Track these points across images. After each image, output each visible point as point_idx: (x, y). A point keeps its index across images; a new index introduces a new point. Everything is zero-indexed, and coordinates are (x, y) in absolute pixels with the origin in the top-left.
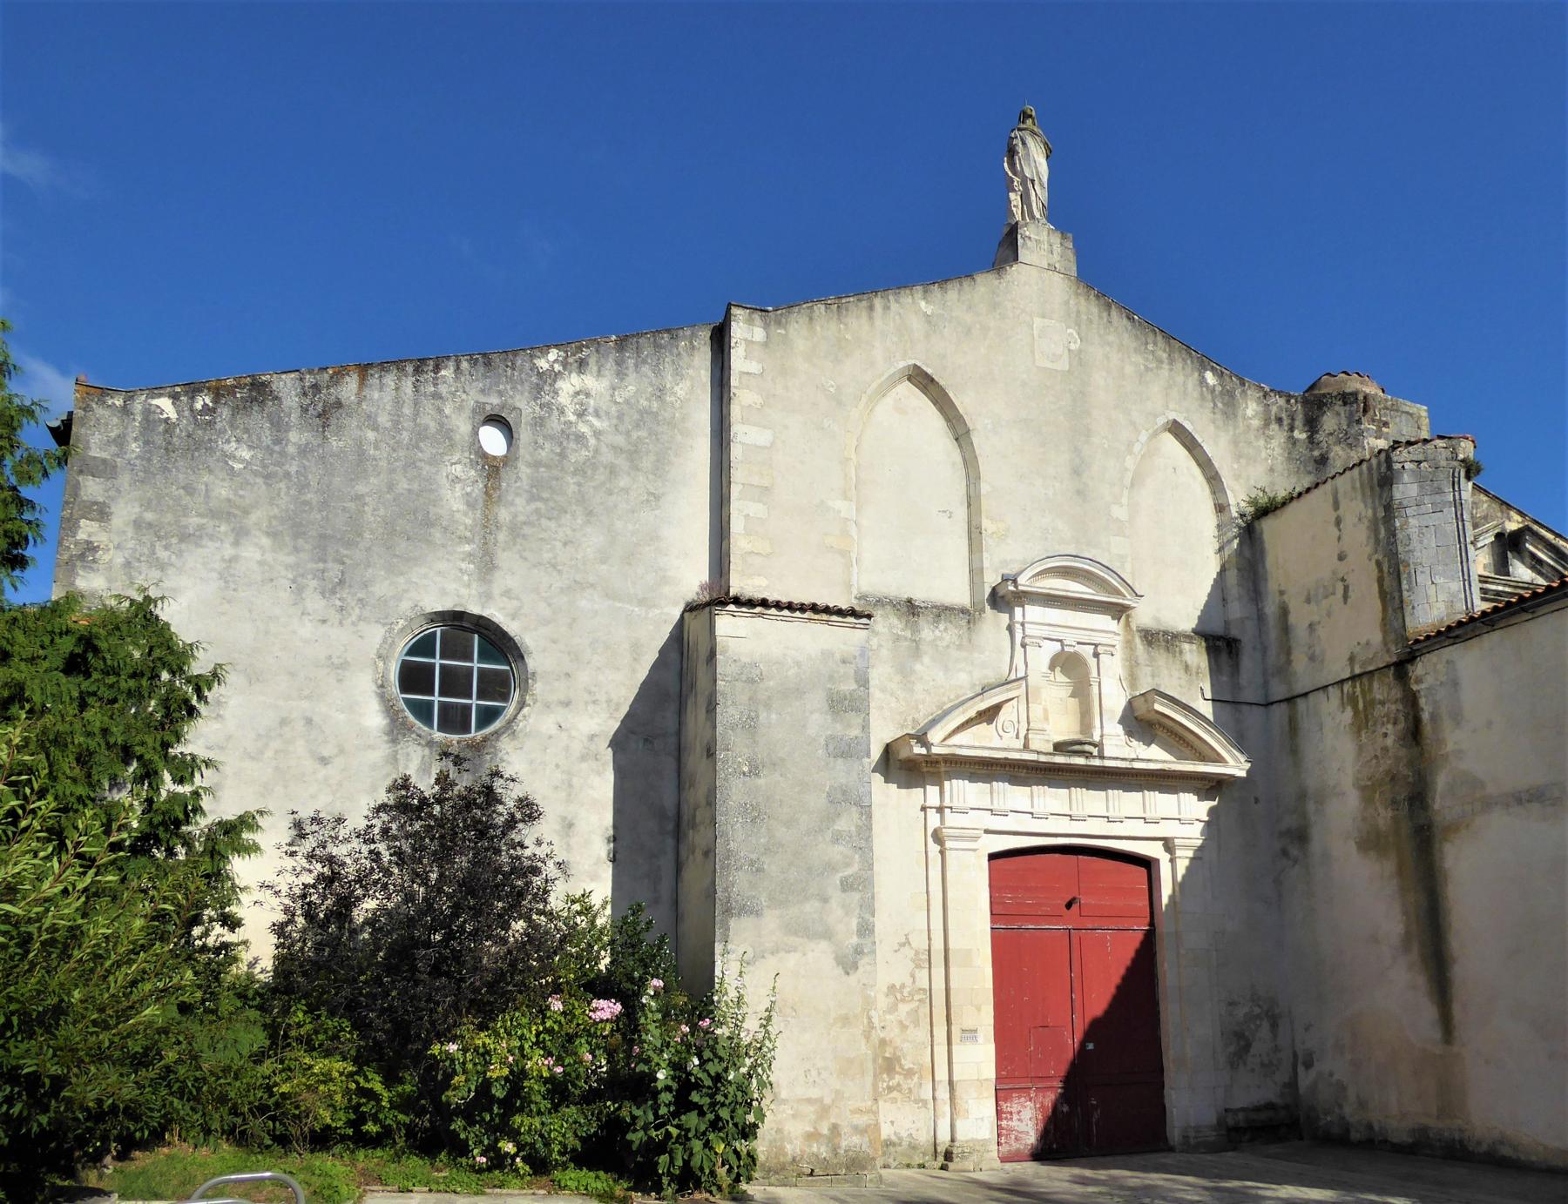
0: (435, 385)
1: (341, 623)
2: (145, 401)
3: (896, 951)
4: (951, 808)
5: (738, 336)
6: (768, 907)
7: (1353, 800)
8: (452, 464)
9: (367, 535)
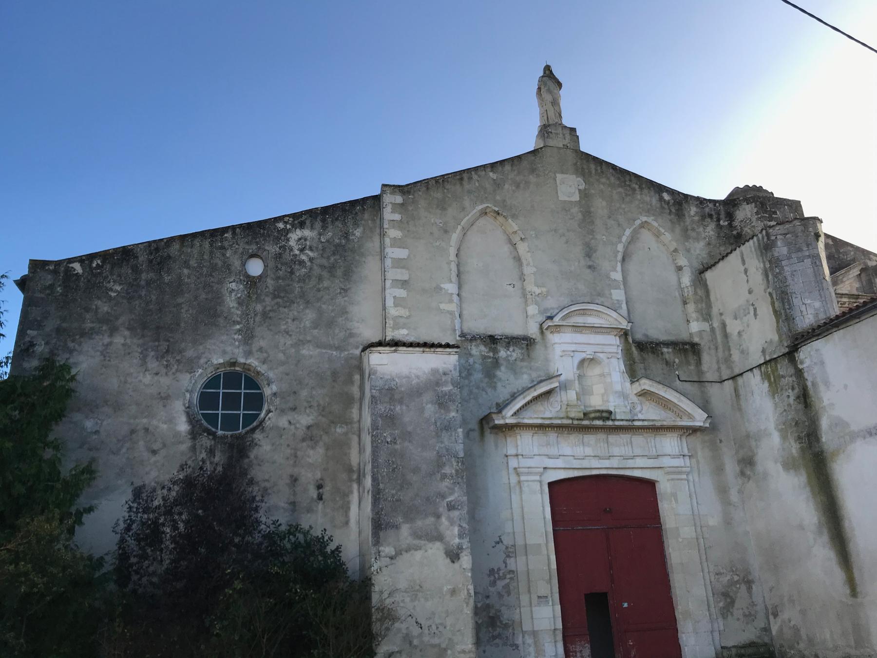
0: (221, 242)
1: (166, 374)
2: (66, 265)
3: (493, 547)
4: (522, 455)
5: (388, 201)
6: (403, 522)
7: (776, 438)
8: (230, 283)
9: (182, 325)
